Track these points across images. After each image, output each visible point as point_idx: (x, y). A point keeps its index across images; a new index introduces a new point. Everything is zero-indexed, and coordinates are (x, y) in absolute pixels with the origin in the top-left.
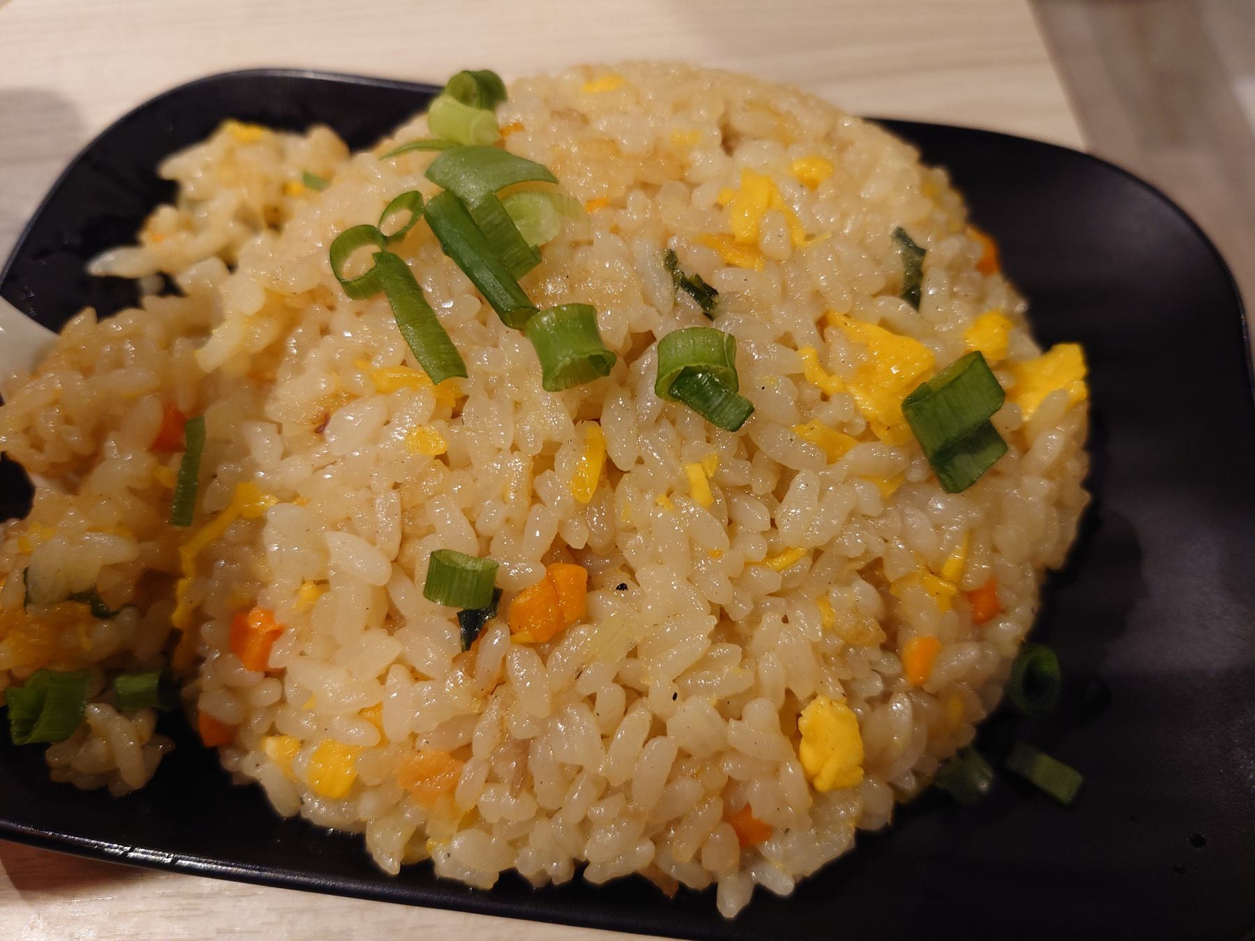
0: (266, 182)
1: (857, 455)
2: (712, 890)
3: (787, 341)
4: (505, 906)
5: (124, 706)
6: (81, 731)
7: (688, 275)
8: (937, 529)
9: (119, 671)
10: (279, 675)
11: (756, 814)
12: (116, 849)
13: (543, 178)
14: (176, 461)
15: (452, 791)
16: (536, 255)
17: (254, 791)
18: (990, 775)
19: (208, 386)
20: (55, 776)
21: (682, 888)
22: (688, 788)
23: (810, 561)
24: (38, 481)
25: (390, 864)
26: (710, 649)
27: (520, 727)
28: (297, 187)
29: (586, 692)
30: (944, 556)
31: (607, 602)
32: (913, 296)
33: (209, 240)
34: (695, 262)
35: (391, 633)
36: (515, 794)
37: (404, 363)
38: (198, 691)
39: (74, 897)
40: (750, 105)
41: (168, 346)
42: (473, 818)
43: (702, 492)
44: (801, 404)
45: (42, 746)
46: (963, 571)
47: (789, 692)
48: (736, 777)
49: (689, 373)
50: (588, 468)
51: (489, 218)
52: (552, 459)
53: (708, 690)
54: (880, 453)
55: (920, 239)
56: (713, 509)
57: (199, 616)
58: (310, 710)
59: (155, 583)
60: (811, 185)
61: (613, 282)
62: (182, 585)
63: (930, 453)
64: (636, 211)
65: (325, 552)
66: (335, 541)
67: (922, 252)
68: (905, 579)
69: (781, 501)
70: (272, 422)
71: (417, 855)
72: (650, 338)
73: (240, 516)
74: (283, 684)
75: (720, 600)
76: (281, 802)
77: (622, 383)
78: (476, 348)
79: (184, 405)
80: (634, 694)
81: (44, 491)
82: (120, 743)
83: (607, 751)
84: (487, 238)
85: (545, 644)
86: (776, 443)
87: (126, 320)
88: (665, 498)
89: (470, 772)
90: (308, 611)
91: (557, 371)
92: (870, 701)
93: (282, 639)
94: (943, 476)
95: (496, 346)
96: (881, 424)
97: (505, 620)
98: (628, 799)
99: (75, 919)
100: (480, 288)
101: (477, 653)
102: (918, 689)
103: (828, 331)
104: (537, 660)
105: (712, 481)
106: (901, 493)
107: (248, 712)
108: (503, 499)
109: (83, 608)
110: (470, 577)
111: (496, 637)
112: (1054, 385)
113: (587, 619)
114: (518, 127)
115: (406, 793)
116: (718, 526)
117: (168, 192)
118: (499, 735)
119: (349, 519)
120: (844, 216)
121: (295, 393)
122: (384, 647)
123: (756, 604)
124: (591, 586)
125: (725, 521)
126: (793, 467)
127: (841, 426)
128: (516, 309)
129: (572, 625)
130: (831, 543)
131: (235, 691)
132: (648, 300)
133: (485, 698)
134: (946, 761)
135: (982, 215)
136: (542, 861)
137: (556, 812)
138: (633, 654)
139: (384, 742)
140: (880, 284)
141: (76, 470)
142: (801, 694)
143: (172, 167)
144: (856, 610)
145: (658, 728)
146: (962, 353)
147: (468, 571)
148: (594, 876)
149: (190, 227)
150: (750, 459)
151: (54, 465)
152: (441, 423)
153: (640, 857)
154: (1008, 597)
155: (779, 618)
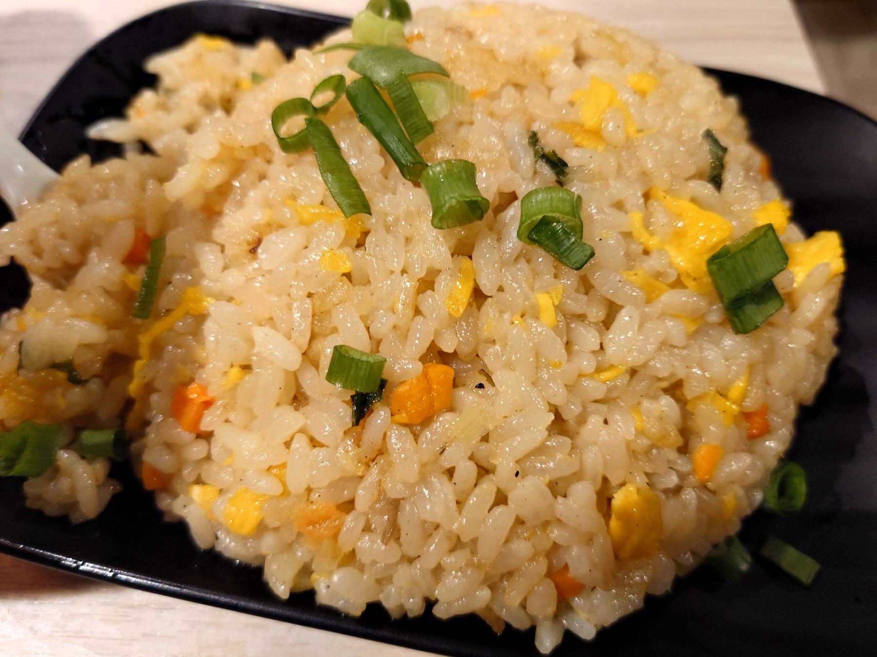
0: (224, 79)
1: (669, 298)
2: (532, 632)
3: (619, 205)
4: (370, 631)
5: (86, 454)
6: (53, 471)
7: (547, 150)
8: (723, 361)
9: (83, 428)
10: (207, 437)
11: (572, 573)
12: (70, 562)
13: (440, 72)
14: (141, 273)
15: (335, 536)
16: (431, 127)
17: (181, 527)
18: (749, 559)
19: (170, 215)
20: (30, 504)
21: (508, 626)
22: (521, 547)
23: (628, 377)
24: (34, 278)
25: (282, 590)
26: (547, 440)
27: (395, 490)
28: (246, 83)
29: (447, 465)
30: (731, 382)
31: (467, 397)
32: (717, 181)
33: (180, 117)
34: (551, 141)
35: (296, 409)
36: (385, 542)
37: (322, 203)
38: (144, 446)
39: (36, 599)
40: (598, 34)
41: (143, 188)
42: (350, 558)
43: (549, 316)
44: (628, 255)
45: (21, 480)
46: (744, 396)
47: (605, 480)
48: (559, 542)
49: (545, 222)
50: (462, 291)
51: (399, 92)
52: (433, 282)
53: (543, 471)
54: (687, 299)
55: (724, 141)
56: (556, 329)
57: (149, 388)
58: (229, 466)
59: (118, 362)
60: (642, 94)
61: (491, 153)
62: (139, 364)
63: (726, 300)
64: (507, 101)
65: (251, 343)
66: (260, 334)
67: (725, 150)
68: (700, 398)
69: (608, 329)
70: (217, 244)
71: (303, 586)
72: (513, 197)
73: (187, 313)
74: (209, 444)
75: (558, 401)
76: (201, 537)
77: (491, 229)
78: (379, 195)
79: (151, 230)
80: (484, 471)
81: (39, 287)
82: (80, 482)
83: (460, 512)
84: (395, 110)
85: (418, 425)
86: (609, 280)
87: (110, 167)
88: (519, 318)
89: (352, 523)
90: (234, 388)
91: (445, 210)
92: (666, 491)
93: (212, 409)
94: (736, 320)
95: (394, 193)
96: (688, 275)
97: (388, 404)
98: (474, 553)
99: (36, 616)
100: (385, 147)
101: (363, 428)
102: (703, 487)
103: (651, 202)
104: (411, 437)
105: (558, 308)
106: (700, 330)
107: (181, 464)
108: (393, 311)
109: (62, 375)
110: (364, 367)
111: (380, 416)
112: (817, 262)
113: (451, 409)
114: (420, 37)
115: (299, 535)
116: (560, 344)
117: (152, 81)
118: (376, 493)
119: (271, 319)
120: (666, 118)
121: (236, 223)
122: (291, 419)
123: (584, 408)
124: (456, 384)
125: (565, 340)
126: (619, 302)
127: (658, 275)
128: (413, 164)
129: (440, 412)
130: (645, 365)
131: (170, 447)
132: (514, 166)
133: (368, 466)
134: (715, 546)
135: (758, 137)
136: (401, 597)
137: (415, 559)
138: (485, 439)
139: (286, 493)
140: (692, 171)
141: (64, 275)
142: (614, 481)
143: (157, 64)
144: (661, 419)
145: (501, 499)
146: (751, 228)
147: (363, 361)
148: (441, 612)
149: (164, 107)
150: (586, 293)
151: (49, 269)
152: (348, 250)
153: (479, 600)
154: (776, 420)
155: (602, 420)
